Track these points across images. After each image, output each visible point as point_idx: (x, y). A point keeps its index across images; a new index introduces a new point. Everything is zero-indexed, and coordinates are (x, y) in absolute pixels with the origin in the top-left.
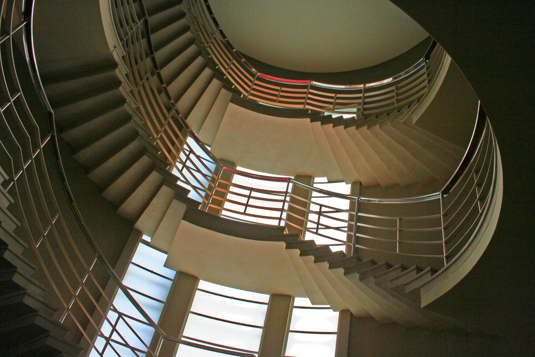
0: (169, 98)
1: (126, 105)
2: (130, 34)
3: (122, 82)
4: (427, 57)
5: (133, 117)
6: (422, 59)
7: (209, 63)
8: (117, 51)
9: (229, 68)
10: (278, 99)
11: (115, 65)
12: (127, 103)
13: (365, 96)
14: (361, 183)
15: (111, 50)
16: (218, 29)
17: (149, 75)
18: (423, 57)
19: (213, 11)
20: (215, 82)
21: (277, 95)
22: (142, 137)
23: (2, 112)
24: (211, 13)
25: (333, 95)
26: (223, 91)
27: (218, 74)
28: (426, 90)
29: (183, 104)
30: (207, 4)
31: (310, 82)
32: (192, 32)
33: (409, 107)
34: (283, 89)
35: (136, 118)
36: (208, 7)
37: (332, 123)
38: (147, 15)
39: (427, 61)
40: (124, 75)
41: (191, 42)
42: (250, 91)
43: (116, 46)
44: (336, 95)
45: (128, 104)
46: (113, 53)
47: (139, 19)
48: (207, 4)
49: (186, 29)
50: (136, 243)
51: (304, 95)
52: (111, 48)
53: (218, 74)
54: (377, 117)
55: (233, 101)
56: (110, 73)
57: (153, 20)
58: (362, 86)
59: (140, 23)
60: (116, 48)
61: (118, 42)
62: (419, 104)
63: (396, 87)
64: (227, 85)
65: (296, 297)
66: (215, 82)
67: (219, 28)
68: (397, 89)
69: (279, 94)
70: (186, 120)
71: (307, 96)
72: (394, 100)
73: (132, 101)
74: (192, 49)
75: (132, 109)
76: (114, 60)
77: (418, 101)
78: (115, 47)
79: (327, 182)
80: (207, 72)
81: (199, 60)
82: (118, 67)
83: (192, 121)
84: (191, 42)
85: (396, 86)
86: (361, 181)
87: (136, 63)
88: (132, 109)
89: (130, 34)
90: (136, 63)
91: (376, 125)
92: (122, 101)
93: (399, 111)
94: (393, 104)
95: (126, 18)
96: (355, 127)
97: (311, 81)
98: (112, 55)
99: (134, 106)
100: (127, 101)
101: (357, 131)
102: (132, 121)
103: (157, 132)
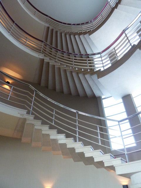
0: (60, 51)
5: (61, 67)
7: (75, 34)
20: (77, 37)
23: (54, 125)
24: (65, 24)
26: (85, 36)
29: (83, 52)
30: (85, 23)
32: (63, 33)
41: (66, 35)
48: (85, 23)
55: (90, 35)
64: (85, 33)
74: (68, 36)
76: (42, 59)
78: (39, 55)
80: (72, 37)
83: (89, 52)
87: (51, 54)
90: (51, 54)
92: (48, 63)
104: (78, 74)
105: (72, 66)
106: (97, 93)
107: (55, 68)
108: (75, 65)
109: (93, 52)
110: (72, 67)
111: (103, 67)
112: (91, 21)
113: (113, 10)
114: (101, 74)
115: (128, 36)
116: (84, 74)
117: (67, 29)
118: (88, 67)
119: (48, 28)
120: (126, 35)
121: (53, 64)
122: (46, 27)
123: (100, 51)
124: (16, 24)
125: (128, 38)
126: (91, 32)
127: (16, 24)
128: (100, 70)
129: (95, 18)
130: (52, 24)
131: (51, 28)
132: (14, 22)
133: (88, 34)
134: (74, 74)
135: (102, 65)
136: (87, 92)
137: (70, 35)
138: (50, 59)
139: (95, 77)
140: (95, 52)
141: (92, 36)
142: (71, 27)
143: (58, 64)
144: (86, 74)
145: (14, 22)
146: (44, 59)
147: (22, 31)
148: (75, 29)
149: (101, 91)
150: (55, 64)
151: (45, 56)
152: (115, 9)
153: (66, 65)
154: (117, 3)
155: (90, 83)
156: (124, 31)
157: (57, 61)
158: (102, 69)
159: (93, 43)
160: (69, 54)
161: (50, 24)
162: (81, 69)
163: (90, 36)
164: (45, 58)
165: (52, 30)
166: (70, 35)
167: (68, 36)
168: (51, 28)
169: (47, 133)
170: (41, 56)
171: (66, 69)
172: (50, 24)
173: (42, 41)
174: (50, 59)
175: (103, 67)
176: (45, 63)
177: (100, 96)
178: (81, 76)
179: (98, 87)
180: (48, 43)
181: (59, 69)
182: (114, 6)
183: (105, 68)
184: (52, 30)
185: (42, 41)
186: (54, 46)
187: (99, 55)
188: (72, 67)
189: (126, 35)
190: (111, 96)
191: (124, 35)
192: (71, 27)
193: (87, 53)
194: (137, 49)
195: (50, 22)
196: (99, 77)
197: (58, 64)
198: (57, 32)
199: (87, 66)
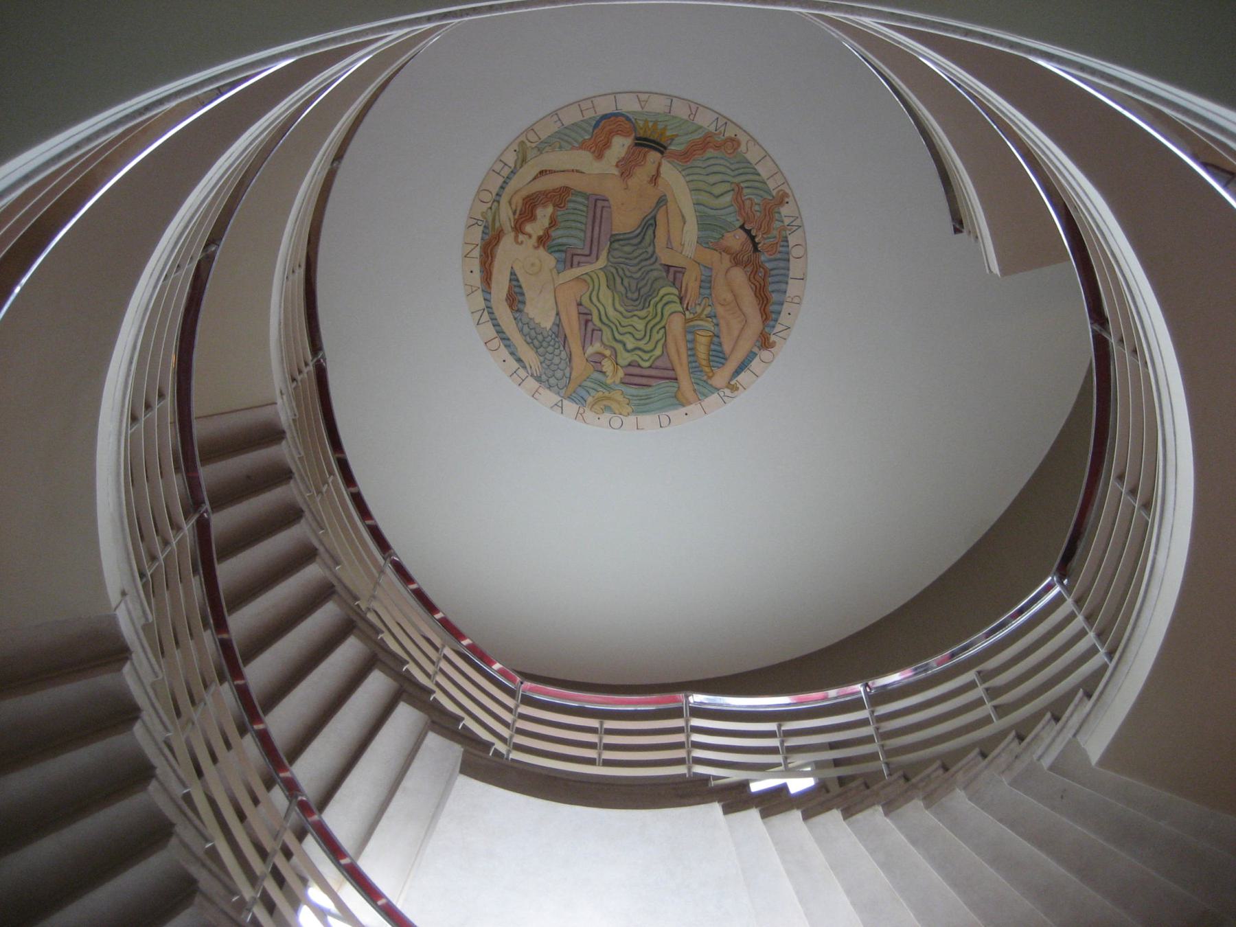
1: (153, 786)
2: (162, 558)
3: (143, 710)
4: (1063, 571)
5: (179, 829)
6: (1050, 578)
8: (131, 606)
9: (438, 671)
10: (600, 755)
11: (118, 653)
12: (157, 779)
13: (876, 714)
15: (114, 604)
16: (388, 560)
18: (1052, 572)
21: (596, 744)
22: (209, 899)
24: (364, 512)
25: (771, 726)
28: (1100, 658)
31: (687, 697)
33: (1057, 719)
34: (610, 724)
35: (184, 831)
37: (798, 808)
38: (207, 506)
41: (322, 593)
42: (511, 737)
43: (126, 591)
44: (779, 726)
45: (161, 784)
46: (118, 612)
47: (187, 516)
49: (305, 555)
51: (679, 738)
52: (113, 595)
54: (945, 768)
56: (103, 680)
57: (223, 521)
58: (859, 687)
59: (188, 528)
60: (128, 598)
61: (134, 580)
62: (1094, 705)
63: (979, 672)
66: (405, 717)
67: (390, 556)
68: (985, 676)
69: (601, 740)
71: (688, 739)
72: (988, 708)
73: (172, 774)
74: (325, 616)
75: (173, 800)
77: (1089, 695)
78: (124, 594)
81: (349, 651)
82: (131, 659)
84: (322, 593)
85: (978, 668)
88: (173, 800)
89: (162, 558)
91: (954, 789)
93: (1021, 738)
94: (987, 720)
96: (880, 809)
97: (688, 694)
98: (113, 620)
99: (179, 791)
101: (891, 819)
102: (174, 841)
103: (253, 878)
122: (263, 415)
131: (286, 452)
141: (471, 789)
165: (280, 475)
167: (325, 616)
168: (286, 452)
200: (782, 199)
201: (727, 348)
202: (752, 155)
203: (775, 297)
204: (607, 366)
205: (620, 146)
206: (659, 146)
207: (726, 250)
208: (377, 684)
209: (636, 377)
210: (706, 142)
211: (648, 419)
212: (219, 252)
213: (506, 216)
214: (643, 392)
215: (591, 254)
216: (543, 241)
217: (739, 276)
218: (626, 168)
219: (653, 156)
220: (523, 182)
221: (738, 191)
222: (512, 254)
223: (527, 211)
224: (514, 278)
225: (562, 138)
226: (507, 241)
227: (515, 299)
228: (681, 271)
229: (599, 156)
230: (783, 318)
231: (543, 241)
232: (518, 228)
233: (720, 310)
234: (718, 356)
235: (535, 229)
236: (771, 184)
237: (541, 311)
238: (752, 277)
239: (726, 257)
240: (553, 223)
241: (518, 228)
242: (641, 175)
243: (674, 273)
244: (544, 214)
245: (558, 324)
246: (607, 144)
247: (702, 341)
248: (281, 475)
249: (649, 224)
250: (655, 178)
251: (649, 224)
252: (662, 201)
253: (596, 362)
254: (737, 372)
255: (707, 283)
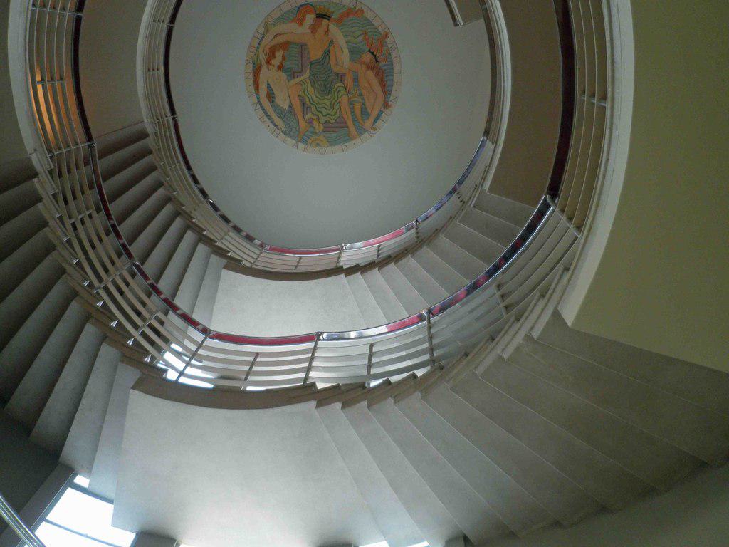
5: (59, 248)
7: (190, 226)
14: (466, 538)
17: (93, 211)
19: (192, 166)
24: (196, 181)
26: (214, 258)
27: (202, 238)
36: (194, 177)
39: (556, 202)
40: (50, 194)
41: (168, 200)
50: (58, 488)
53: (202, 238)
64: (221, 253)
65: (115, 509)
66: (202, 249)
70: (157, 284)
74: (168, 209)
78: (35, 150)
79: (481, 22)
81: (178, 223)
83: (181, 301)
84: (168, 200)
86: (466, 533)
95: (77, 160)
98: (29, 159)
100: (50, 224)
104: (87, 317)
105: (96, 283)
106: (74, 447)
107: (41, 234)
108: (106, 289)
109: (192, 312)
110: (91, 285)
111: (181, 374)
112: (262, 246)
113: (336, 271)
114: (154, 383)
115: (314, 364)
116: (104, 338)
117: (186, 198)
118: (136, 334)
119: (144, 135)
120: (314, 349)
121: (47, 216)
123: (216, 327)
124: (78, 20)
125: (312, 359)
126: (235, 265)
127: (78, 20)
128: (165, 371)
129: (283, 251)
130: (162, 137)
132: (173, 20)
133: (225, 261)
134: (74, 307)
135: (177, 374)
136: (45, 411)
137: (177, 214)
138: (55, 196)
139: (129, 374)
140: (195, 316)
141: (229, 277)
142: (201, 202)
143: (59, 233)
144: (113, 343)
145: (173, 20)
146: (36, 175)
147: (71, 46)
148: (202, 217)
149: (95, 451)
150: (51, 223)
151: (50, 172)
152: (343, 275)
153: (79, 264)
154: (358, 266)
155: (95, 385)
156: (314, 337)
157: (68, 223)
158: (171, 375)
159: (212, 299)
160: (125, 251)
161: (156, 133)
162: (113, 318)
163: (224, 271)
164: (44, 176)
165: (147, 152)
166: (177, 214)
168: (150, 142)
169: (519, 339)
170: (39, 161)
171: (69, 269)
172: (156, 133)
173: (89, 138)
174: (55, 196)
175: (181, 374)
176: (27, 185)
177: (77, 467)
178: (90, 330)
179: (101, 427)
180: (103, 164)
181: (49, 248)
182: (345, 267)
183: (183, 380)
184: (147, 152)
185: (89, 138)
186: (108, 186)
187: (199, 337)
188: (91, 285)
189: (314, 349)
190: (110, 501)
191: (311, 345)
192: (201, 202)
193: (174, 295)
194: (310, 400)
195: (165, 131)
196: (138, 386)
197: (59, 233)
198: (152, 168)
199: (136, 327)
200: (386, 36)
201: (369, 111)
202: (370, 16)
203: (388, 83)
204: (315, 123)
205: (310, 18)
206: (321, 16)
207: (364, 63)
208: (189, 237)
209: (328, 128)
210: (349, 13)
211: (336, 148)
212: (176, 26)
213: (262, 58)
214: (333, 134)
215: (301, 72)
216: (280, 67)
217: (370, 74)
218: (314, 29)
219: (325, 22)
220: (268, 41)
221: (365, 34)
222: (267, 75)
223: (271, 54)
224: (269, 87)
225: (284, 18)
226: (264, 70)
227: (271, 96)
228: (344, 75)
229: (301, 24)
230: (393, 93)
231: (280, 67)
232: (268, 62)
233: (363, 91)
234: (365, 113)
235: (276, 62)
236: (380, 29)
237: (283, 101)
238: (377, 74)
239: (364, 66)
240: (284, 58)
241: (268, 62)
242: (321, 30)
243: (341, 76)
244: (279, 54)
245: (291, 107)
246: (304, 19)
247: (357, 107)
248: (148, 152)
249: (327, 54)
250: (327, 32)
251: (327, 54)
252: (331, 42)
253: (310, 122)
254: (375, 121)
255: (356, 80)
